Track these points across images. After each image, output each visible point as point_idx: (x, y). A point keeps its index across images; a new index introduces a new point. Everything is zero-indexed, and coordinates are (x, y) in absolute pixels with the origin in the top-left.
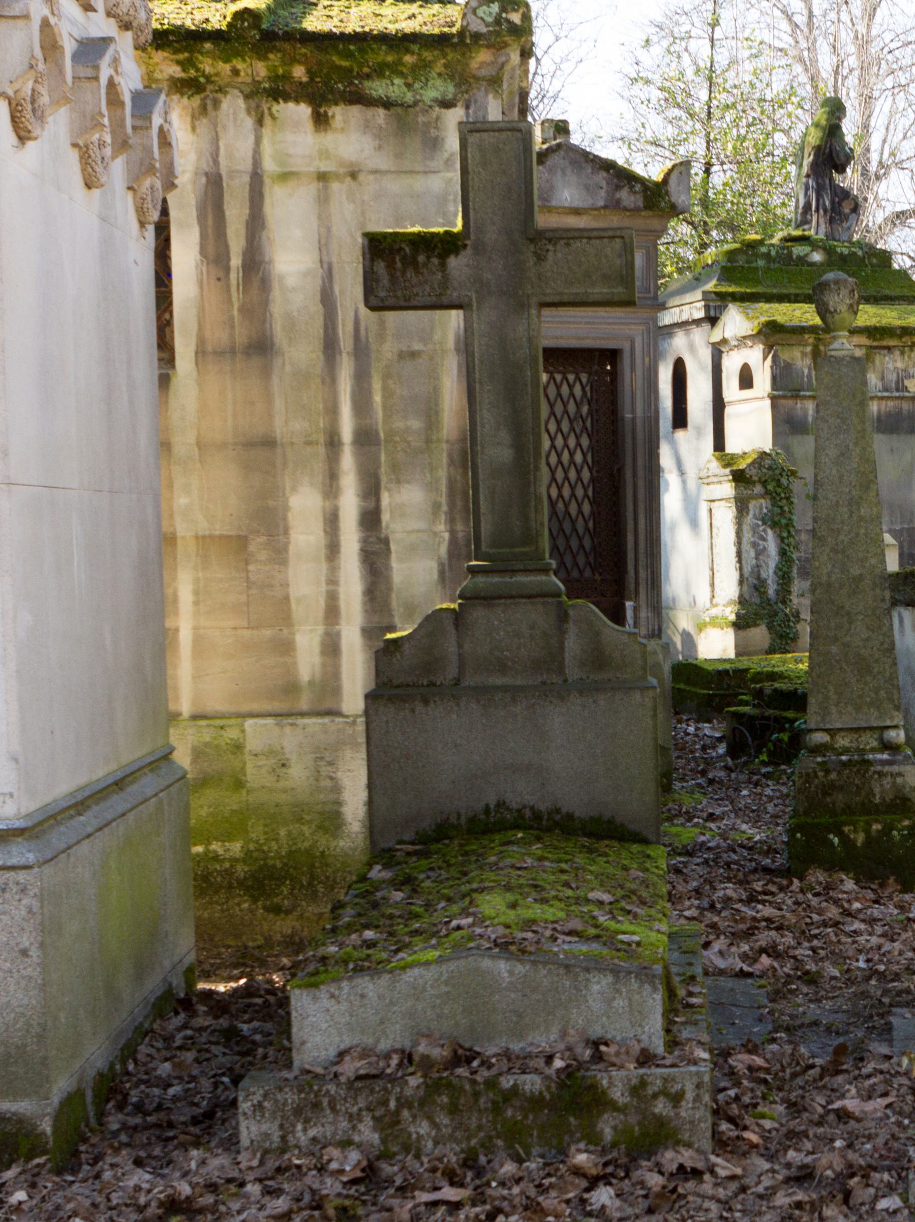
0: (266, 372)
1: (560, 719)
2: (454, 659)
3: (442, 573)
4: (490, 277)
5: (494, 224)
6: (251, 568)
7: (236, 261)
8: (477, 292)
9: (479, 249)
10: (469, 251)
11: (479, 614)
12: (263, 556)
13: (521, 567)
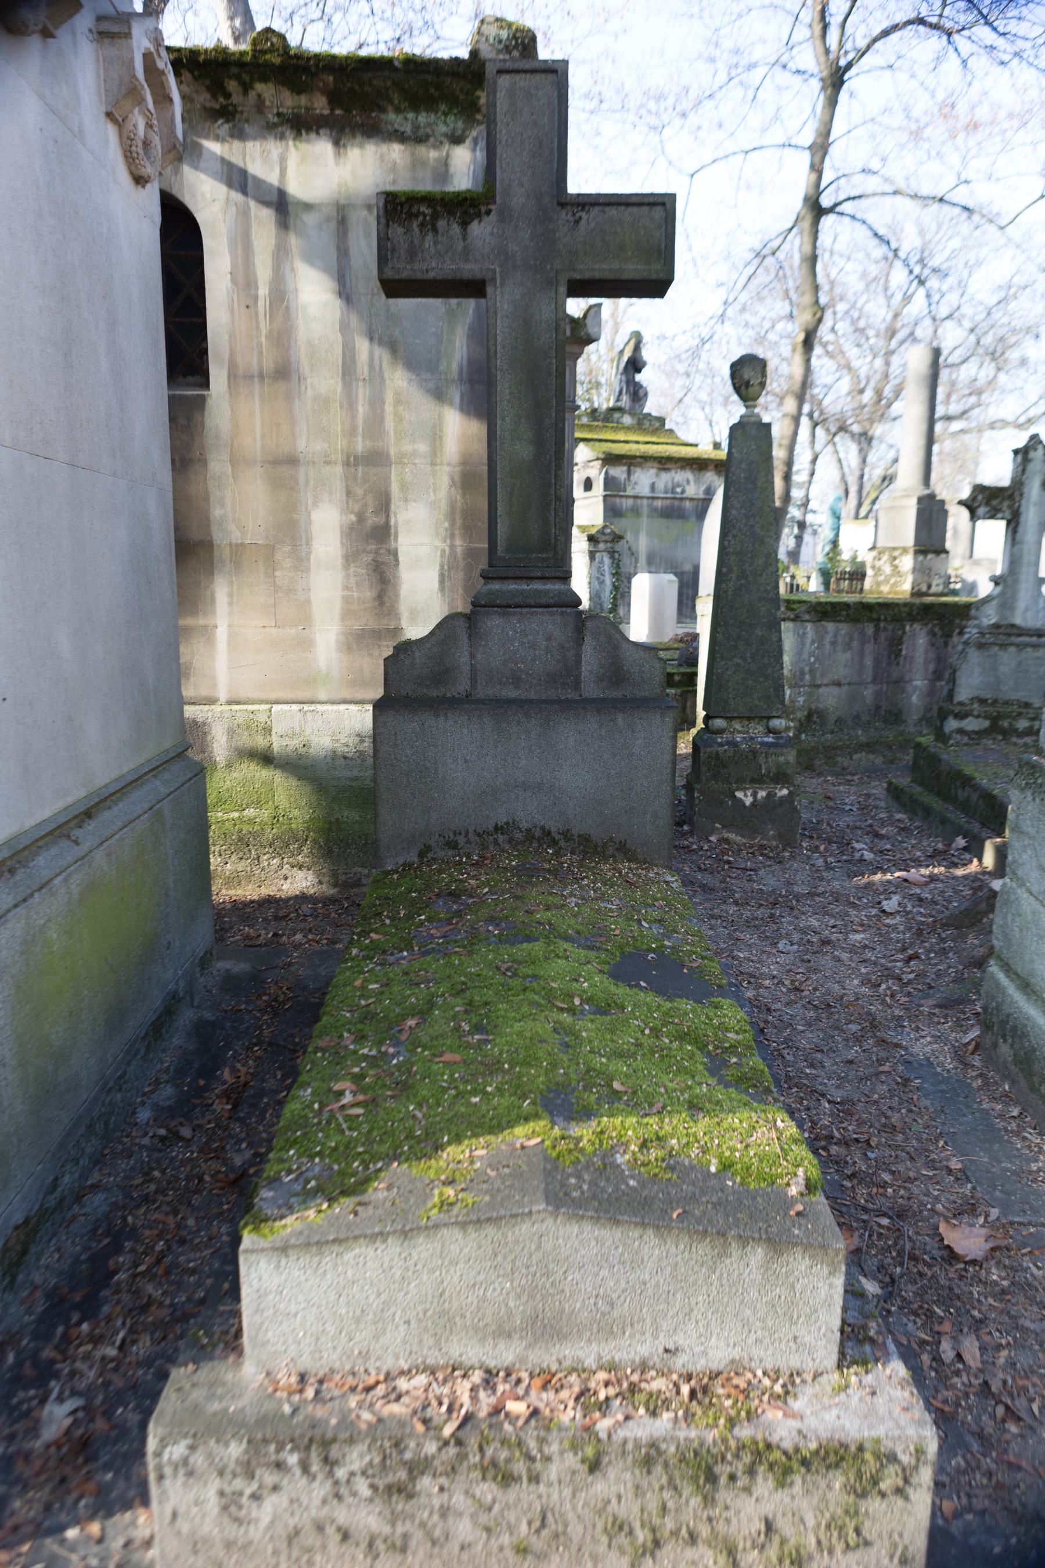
0: (289, 398)
1: (572, 735)
2: (467, 669)
3: (442, 582)
4: (516, 248)
5: (522, 185)
6: (277, 574)
7: (263, 291)
8: (501, 266)
9: (505, 216)
10: (493, 217)
11: (493, 623)
12: (288, 563)
13: (539, 574)
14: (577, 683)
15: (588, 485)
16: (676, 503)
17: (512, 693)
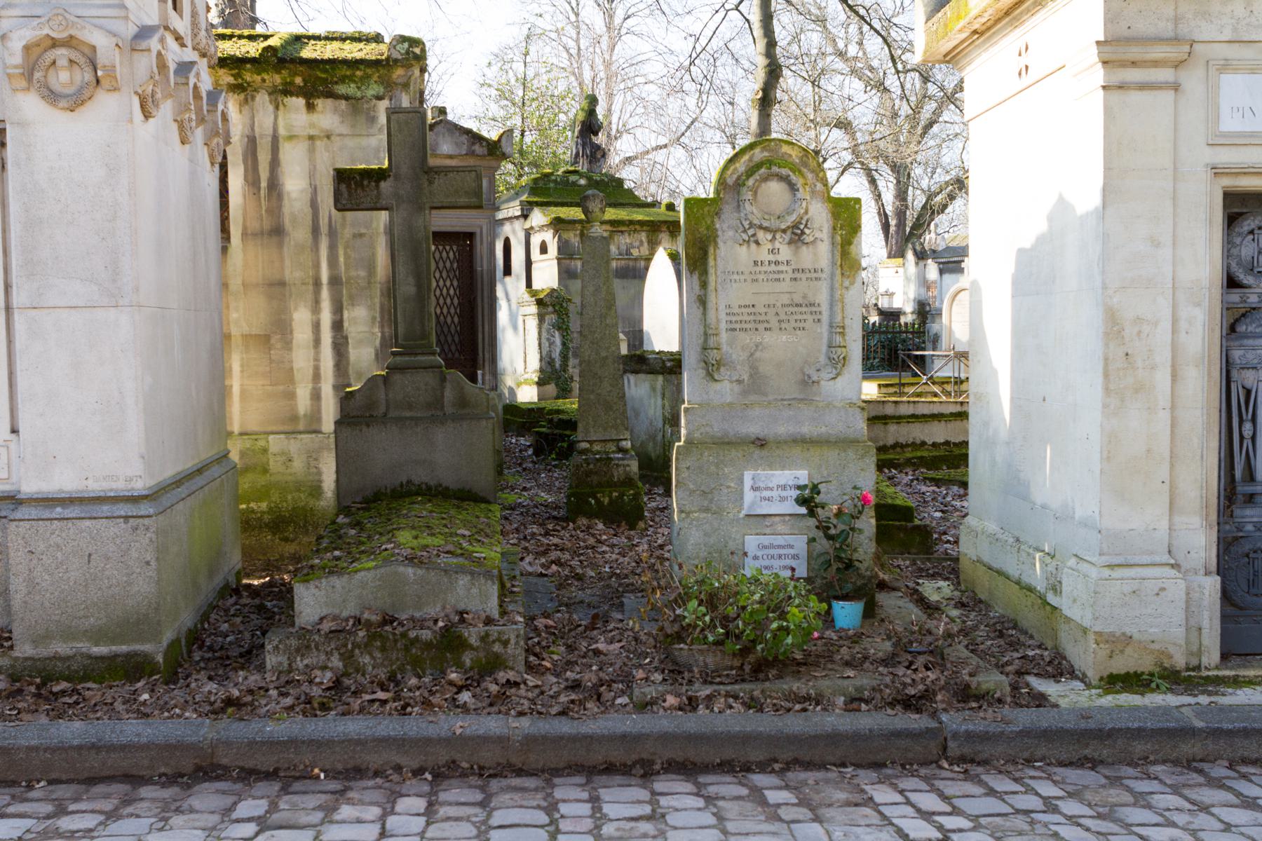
0: (280, 245)
3: (377, 355)
7: (264, 184)
9: (397, 178)
11: (397, 377)
12: (279, 346)
14: (443, 407)
15: (544, 249)
16: (631, 263)
17: (408, 414)
